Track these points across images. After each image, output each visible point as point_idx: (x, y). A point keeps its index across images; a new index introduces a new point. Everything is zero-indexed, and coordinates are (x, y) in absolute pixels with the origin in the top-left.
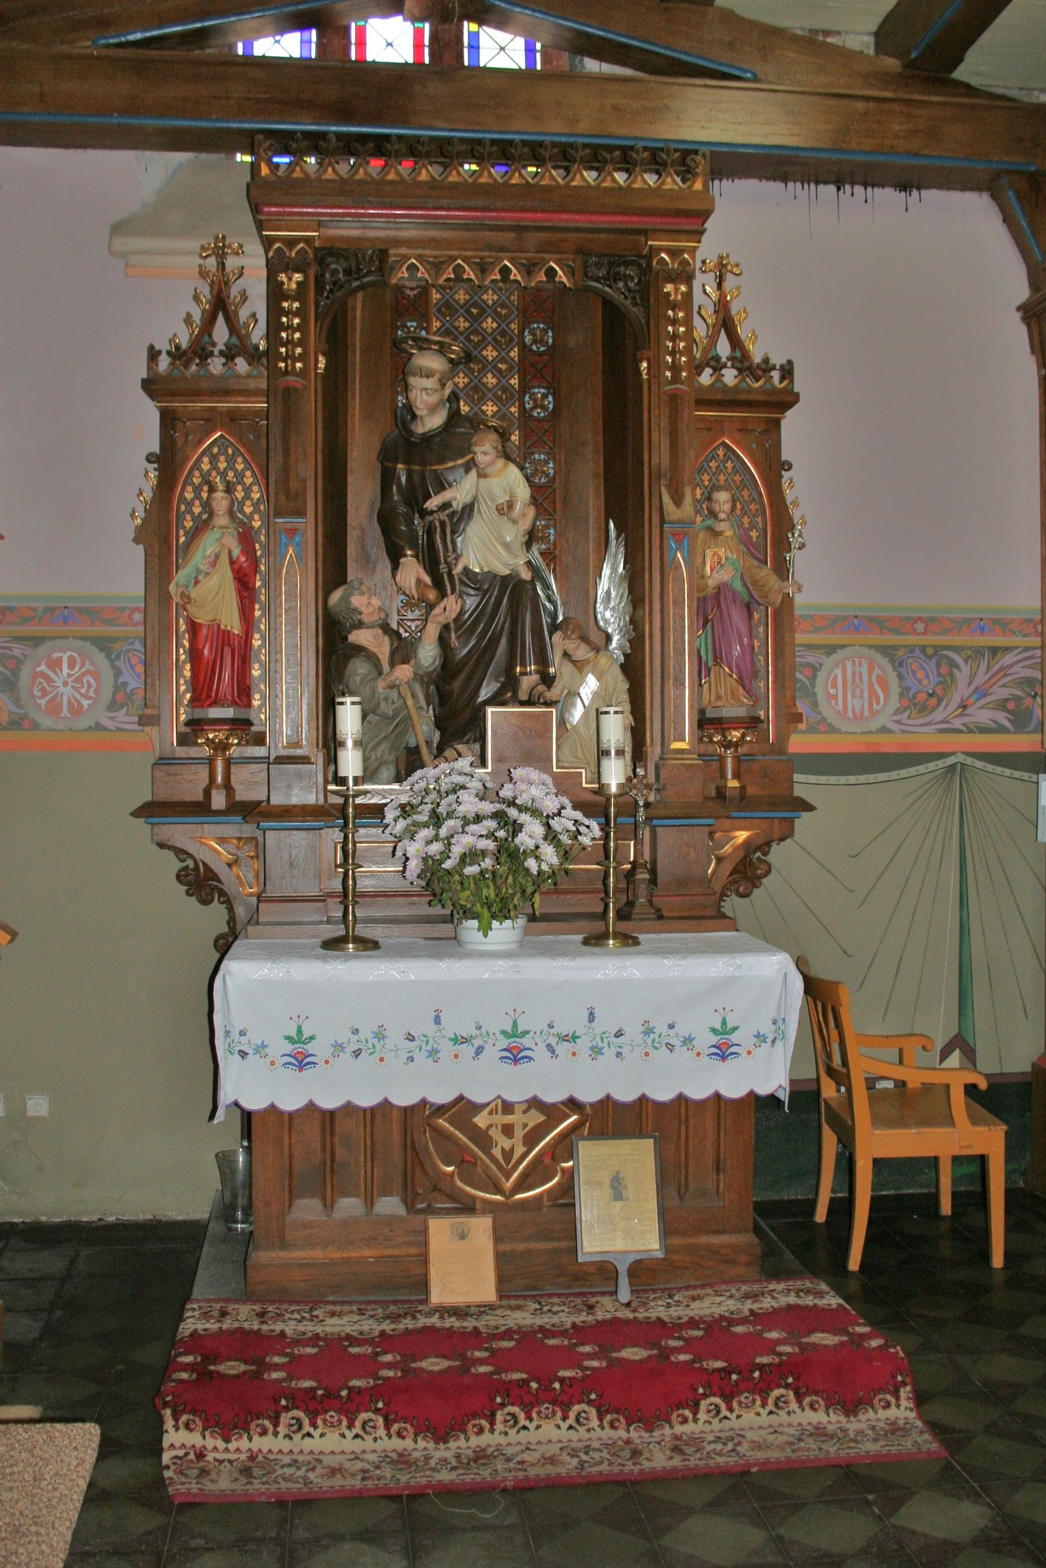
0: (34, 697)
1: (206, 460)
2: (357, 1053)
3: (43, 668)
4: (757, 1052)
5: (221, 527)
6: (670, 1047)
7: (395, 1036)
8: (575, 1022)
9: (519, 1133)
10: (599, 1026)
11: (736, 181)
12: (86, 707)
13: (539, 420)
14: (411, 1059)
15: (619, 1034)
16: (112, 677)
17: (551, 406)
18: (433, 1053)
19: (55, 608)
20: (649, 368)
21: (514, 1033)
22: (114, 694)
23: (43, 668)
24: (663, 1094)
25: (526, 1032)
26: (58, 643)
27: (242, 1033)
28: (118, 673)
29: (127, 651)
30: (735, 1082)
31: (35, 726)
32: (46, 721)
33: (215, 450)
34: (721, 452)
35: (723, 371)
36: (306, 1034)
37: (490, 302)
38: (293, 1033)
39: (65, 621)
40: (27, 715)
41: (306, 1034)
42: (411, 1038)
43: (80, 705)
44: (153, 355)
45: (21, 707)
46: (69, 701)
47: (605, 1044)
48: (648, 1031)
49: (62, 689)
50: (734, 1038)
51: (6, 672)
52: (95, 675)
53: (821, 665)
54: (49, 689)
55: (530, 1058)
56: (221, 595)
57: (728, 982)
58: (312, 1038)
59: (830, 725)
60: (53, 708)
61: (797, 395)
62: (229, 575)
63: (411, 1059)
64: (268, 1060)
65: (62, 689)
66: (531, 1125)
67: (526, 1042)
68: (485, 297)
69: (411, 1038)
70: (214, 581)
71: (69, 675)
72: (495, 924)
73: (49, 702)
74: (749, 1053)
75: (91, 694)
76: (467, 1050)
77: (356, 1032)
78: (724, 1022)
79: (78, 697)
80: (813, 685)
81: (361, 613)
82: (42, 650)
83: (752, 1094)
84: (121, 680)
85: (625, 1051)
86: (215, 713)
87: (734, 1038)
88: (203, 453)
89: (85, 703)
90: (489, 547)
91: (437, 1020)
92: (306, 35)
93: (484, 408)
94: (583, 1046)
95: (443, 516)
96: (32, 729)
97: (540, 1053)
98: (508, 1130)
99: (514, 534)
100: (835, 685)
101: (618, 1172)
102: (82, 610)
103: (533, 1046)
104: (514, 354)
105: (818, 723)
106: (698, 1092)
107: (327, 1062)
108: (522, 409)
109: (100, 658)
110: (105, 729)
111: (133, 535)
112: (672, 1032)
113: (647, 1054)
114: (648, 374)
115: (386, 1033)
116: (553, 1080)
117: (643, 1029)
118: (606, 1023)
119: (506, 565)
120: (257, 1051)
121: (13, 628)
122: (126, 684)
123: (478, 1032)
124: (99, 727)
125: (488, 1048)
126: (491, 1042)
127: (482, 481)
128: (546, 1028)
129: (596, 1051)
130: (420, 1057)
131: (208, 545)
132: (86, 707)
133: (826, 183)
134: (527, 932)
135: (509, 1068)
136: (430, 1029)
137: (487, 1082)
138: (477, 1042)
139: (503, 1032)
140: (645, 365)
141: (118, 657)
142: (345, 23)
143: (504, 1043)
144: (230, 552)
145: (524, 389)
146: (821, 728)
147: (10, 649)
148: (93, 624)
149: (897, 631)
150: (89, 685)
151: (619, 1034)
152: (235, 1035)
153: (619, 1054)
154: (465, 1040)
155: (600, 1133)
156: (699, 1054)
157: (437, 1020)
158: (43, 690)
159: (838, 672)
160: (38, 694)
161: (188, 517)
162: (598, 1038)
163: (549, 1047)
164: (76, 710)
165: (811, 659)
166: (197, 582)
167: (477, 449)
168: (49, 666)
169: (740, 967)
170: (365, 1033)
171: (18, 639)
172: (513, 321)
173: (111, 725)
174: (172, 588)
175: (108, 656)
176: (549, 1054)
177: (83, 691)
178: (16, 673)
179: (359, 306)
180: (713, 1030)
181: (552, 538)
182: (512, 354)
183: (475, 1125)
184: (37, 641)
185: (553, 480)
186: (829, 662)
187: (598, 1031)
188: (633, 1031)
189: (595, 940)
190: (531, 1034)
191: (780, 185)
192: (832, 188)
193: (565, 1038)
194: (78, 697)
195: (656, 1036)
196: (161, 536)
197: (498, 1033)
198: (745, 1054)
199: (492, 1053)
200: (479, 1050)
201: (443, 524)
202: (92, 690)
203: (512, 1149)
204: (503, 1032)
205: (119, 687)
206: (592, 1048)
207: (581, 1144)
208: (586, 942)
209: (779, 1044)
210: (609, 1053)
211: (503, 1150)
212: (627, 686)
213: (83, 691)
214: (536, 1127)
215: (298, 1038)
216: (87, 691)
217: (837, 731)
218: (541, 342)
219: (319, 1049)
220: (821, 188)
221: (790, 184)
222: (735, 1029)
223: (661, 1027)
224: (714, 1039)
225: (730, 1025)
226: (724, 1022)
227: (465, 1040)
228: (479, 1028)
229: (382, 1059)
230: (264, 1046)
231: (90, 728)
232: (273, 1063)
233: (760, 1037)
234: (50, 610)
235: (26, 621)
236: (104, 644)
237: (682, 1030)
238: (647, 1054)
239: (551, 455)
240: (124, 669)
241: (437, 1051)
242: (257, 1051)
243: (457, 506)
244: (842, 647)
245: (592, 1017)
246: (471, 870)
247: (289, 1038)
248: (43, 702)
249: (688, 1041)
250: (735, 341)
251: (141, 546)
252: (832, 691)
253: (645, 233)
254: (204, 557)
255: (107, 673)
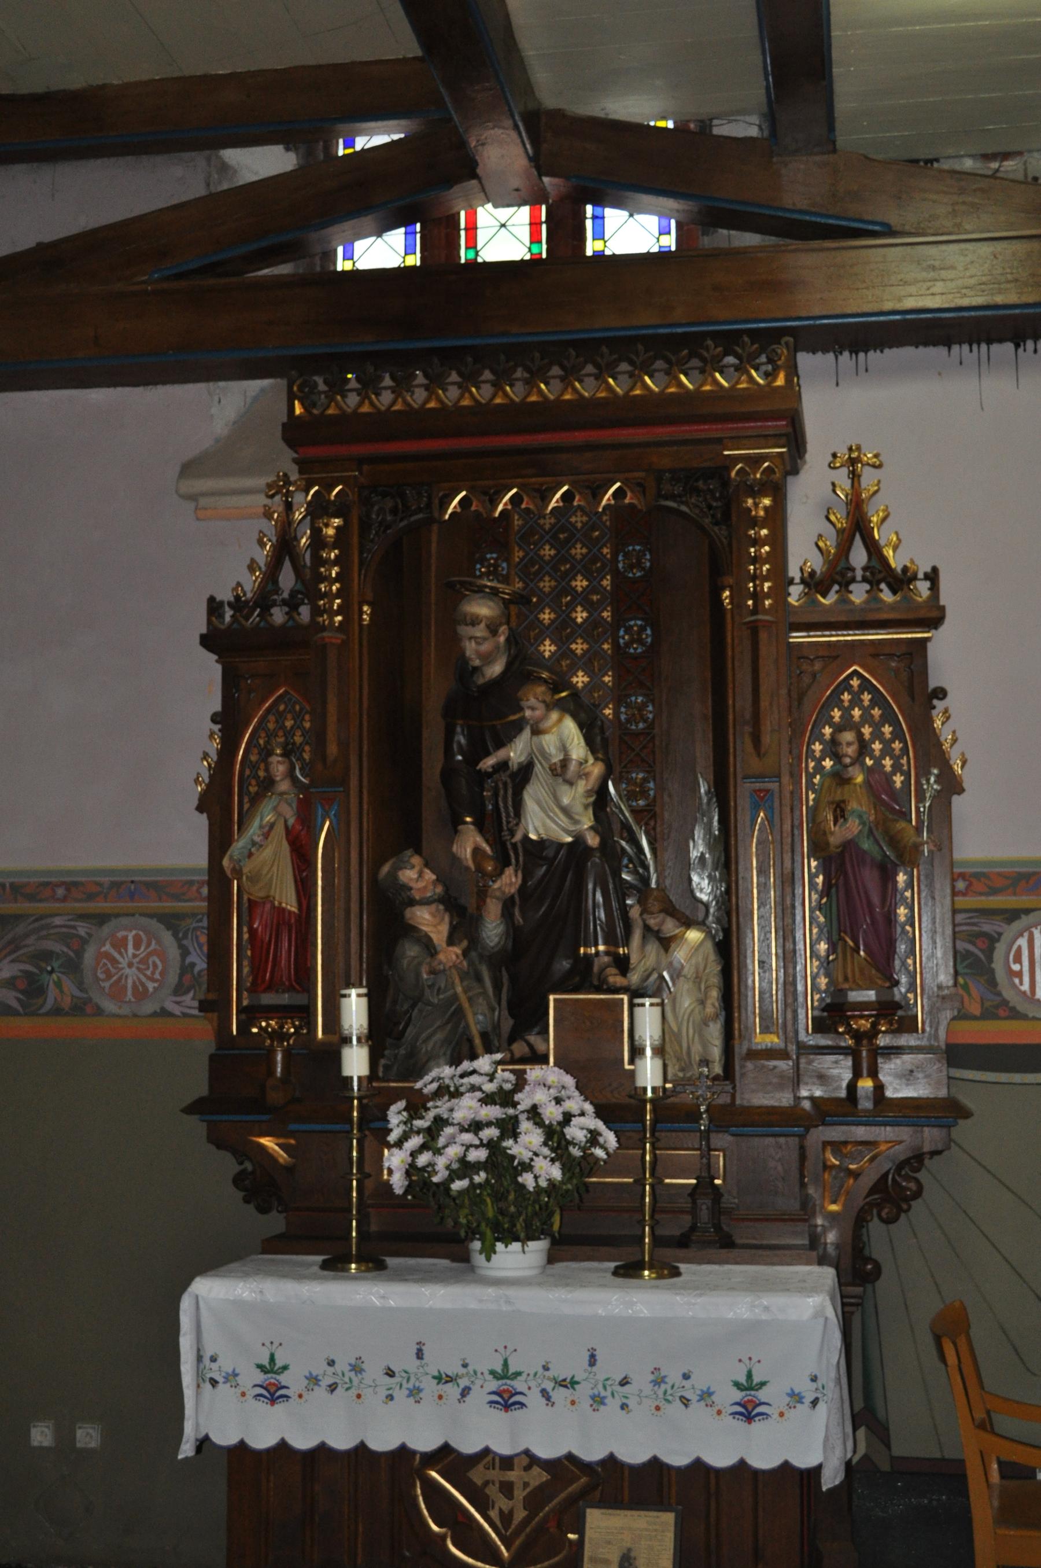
0: (98, 979)
1: (271, 718)
2: (333, 1388)
3: (107, 947)
4: (790, 1414)
5: (282, 794)
6: (685, 1402)
7: (374, 1371)
8: (574, 1366)
9: (519, 1494)
10: (602, 1370)
11: (886, 351)
12: (151, 990)
13: (635, 658)
14: (391, 1397)
15: (624, 1382)
16: (179, 958)
17: (649, 640)
18: (415, 1393)
19: (122, 883)
20: (731, 597)
21: (504, 1374)
22: (181, 975)
23: (107, 947)
24: (678, 1459)
25: (518, 1374)
26: (125, 921)
27: (213, 1359)
28: (185, 952)
29: (195, 929)
30: (765, 1448)
31: (99, 1012)
32: (109, 1006)
33: (282, 707)
34: (855, 682)
35: (852, 587)
36: (279, 1363)
37: (579, 525)
38: (266, 1362)
39: (132, 896)
40: (90, 999)
41: (279, 1363)
42: (390, 1373)
43: (146, 989)
44: (214, 607)
45: (87, 993)
46: (134, 982)
47: (608, 1393)
48: (659, 1382)
49: (127, 971)
50: (762, 1395)
51: (72, 954)
52: (162, 955)
53: (1000, 934)
54: (113, 971)
55: (522, 1405)
56: (275, 869)
57: (753, 1327)
58: (285, 1368)
59: (1013, 1009)
60: (117, 992)
61: (943, 609)
62: (286, 847)
63: (391, 1397)
64: (239, 1391)
65: (127, 971)
66: (534, 1483)
67: (519, 1385)
68: (573, 519)
69: (390, 1373)
70: (267, 853)
71: (135, 956)
72: (500, 1246)
73: (111, 986)
74: (782, 1415)
75: (157, 976)
76: (452, 1391)
77: (331, 1363)
78: (749, 1376)
79: (144, 979)
80: (990, 959)
81: (411, 889)
82: (106, 929)
83: (786, 1465)
84: (188, 960)
85: (632, 1403)
86: (268, 999)
87: (762, 1395)
88: (268, 711)
89: (151, 986)
90: (551, 815)
91: (420, 1354)
92: (410, 229)
93: (573, 646)
94: (584, 1391)
95: (504, 777)
96: (94, 1015)
97: (533, 1399)
98: (507, 1489)
99: (575, 796)
100: (1018, 959)
101: (629, 1550)
102: (148, 885)
103: (525, 1390)
104: (606, 582)
105: (997, 1007)
106: (721, 1459)
107: (300, 1396)
108: (616, 645)
109: (167, 937)
110: (170, 1015)
111: (196, 803)
112: (687, 1384)
113: (658, 1408)
114: (731, 603)
115: (364, 1366)
116: (549, 1433)
117: (652, 1377)
118: (610, 1368)
119: (569, 833)
120: (227, 1379)
121: (77, 905)
122: (193, 965)
123: (464, 1371)
124: (164, 1013)
125: (475, 1389)
126: (479, 1383)
127: (535, 738)
128: (541, 1370)
129: (598, 1401)
130: (400, 1395)
131: (266, 814)
132: (151, 990)
133: (1001, 341)
134: (552, 1259)
135: (498, 1414)
136: (412, 1364)
137: (481, 1431)
138: (463, 1382)
139: (493, 1373)
140: (727, 593)
141: (185, 937)
142: (455, 210)
143: (494, 1385)
144: (286, 821)
145: (619, 621)
146: (1001, 1013)
147: (74, 927)
148: (160, 900)
149: (177, 898)
150: (155, 966)
151: (624, 1382)
152: (206, 1361)
153: (624, 1407)
154: (450, 1379)
155: (613, 1502)
156: (719, 1412)
157: (420, 1354)
158: (109, 976)
159: (1023, 942)
160: (102, 976)
161: (253, 782)
162: (600, 1387)
163: (544, 1393)
164: (141, 994)
165: (986, 928)
166: (250, 855)
167: (524, 704)
168: (113, 946)
169: (767, 1309)
170: (342, 1366)
171: (83, 917)
172: (605, 545)
173: (177, 1010)
174: (226, 862)
175: (175, 935)
176: (544, 1401)
177: (149, 973)
178: (80, 954)
179: (434, 538)
180: (737, 1385)
181: (652, 793)
182: (605, 583)
183: (471, 1481)
184: (101, 919)
185: (651, 726)
186: (1009, 930)
187: (601, 1377)
188: (641, 1381)
189: (629, 1270)
190: (524, 1376)
191: (942, 350)
192: (1009, 346)
193: (562, 1384)
194: (144, 979)
195: (668, 1387)
196: (223, 804)
197: (486, 1373)
198: (776, 1416)
199: (480, 1396)
200: (465, 1392)
201: (505, 784)
202: (157, 972)
203: (511, 1512)
204: (493, 1373)
205: (186, 969)
206: (593, 1398)
207: (589, 1511)
208: (616, 1273)
209: (822, 1406)
210: (613, 1405)
211: (501, 1511)
212: (719, 968)
213: (149, 973)
214: (541, 1488)
215: (271, 1367)
216: (153, 973)
217: (1024, 1017)
218: (639, 565)
219: (293, 1381)
220: (995, 347)
221: (955, 348)
222: (763, 1384)
223: (674, 1377)
224: (738, 1395)
225: (756, 1379)
226: (749, 1376)
227: (450, 1379)
228: (465, 1366)
229: (359, 1396)
230: (235, 1375)
231: (154, 1014)
232: (243, 1394)
233: (796, 1397)
234: (116, 885)
235: (91, 897)
236: (171, 921)
237: (700, 1382)
238: (658, 1408)
239: (650, 699)
240: (191, 949)
241: (419, 1390)
242: (227, 1379)
243: (514, 765)
244: (1028, 911)
245: (593, 1360)
246: (458, 1185)
247: (261, 1367)
248: (106, 985)
249: (706, 1395)
250: (873, 548)
251: (205, 815)
252: (1016, 967)
253: (361, 626)
254: (261, 827)
255: (173, 952)
